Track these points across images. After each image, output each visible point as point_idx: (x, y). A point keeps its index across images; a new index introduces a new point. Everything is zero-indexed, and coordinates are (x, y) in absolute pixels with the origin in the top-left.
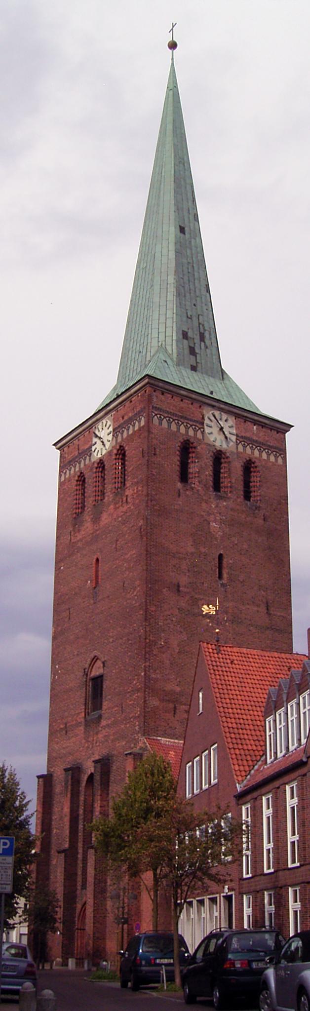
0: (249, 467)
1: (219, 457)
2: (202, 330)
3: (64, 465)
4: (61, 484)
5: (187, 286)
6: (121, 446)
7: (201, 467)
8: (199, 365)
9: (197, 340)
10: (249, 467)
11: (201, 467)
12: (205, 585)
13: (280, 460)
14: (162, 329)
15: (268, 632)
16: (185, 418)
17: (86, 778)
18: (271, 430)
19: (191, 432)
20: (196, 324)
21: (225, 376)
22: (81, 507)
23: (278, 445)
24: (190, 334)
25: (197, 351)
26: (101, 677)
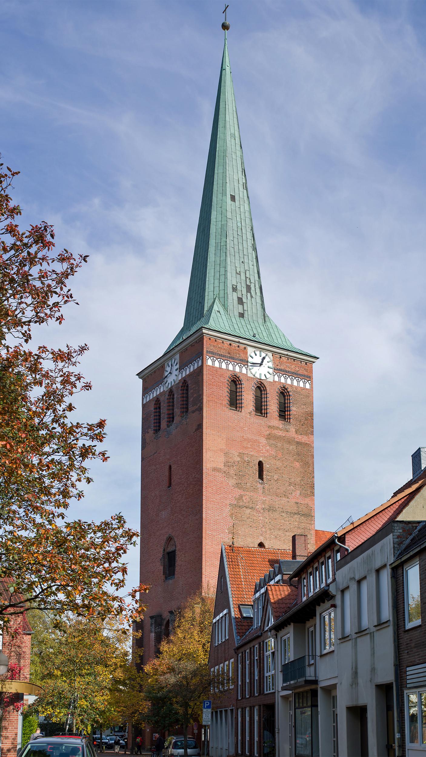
0: (284, 393)
1: (261, 388)
2: (248, 283)
3: (146, 390)
4: (144, 406)
5: (236, 247)
6: (185, 381)
7: (248, 398)
8: (246, 313)
9: (244, 291)
10: (284, 393)
11: (248, 398)
12: (249, 484)
13: (308, 386)
14: (217, 284)
15: (296, 516)
16: (233, 358)
17: (165, 623)
18: (274, 426)
19: (237, 369)
20: (243, 277)
21: (267, 319)
22: (157, 429)
23: (306, 373)
24: (239, 288)
25: (244, 300)
26: (150, 617)
